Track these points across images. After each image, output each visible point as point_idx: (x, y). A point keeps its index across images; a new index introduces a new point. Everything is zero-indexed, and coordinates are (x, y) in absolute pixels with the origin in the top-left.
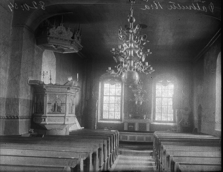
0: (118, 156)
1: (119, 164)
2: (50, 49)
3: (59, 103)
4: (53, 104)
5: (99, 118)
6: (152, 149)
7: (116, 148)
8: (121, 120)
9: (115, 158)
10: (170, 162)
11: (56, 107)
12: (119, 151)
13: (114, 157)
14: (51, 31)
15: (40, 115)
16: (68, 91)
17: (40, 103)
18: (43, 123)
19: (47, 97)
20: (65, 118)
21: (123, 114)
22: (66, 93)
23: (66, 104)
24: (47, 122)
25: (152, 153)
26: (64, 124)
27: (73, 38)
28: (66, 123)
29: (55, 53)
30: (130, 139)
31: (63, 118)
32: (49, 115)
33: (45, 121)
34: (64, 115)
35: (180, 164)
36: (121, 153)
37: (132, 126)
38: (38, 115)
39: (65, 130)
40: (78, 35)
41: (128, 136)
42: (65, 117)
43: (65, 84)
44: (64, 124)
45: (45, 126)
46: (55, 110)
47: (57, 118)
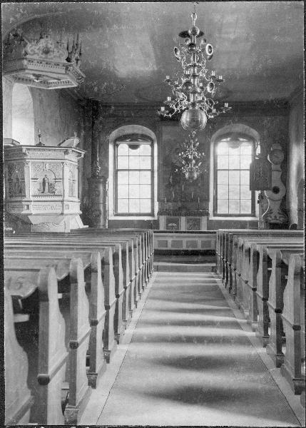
0: (133, 314)
1: (156, 282)
2: (24, 83)
3: (51, 178)
4: (40, 180)
5: (111, 211)
6: (215, 261)
7: (128, 290)
8: (152, 214)
9: (148, 278)
10: (252, 254)
11: (47, 184)
12: (154, 266)
13: (137, 292)
14: (29, 48)
15: (19, 199)
16: (66, 157)
17: (18, 179)
18: (25, 212)
19: (30, 167)
20: (63, 204)
21: (156, 204)
22: (63, 161)
23: (63, 179)
24: (33, 210)
25: (213, 267)
26: (62, 214)
27: (68, 60)
28: (65, 212)
29: (32, 89)
30: (172, 246)
31: (60, 203)
32: (36, 199)
33: (28, 208)
34: (61, 198)
35: (268, 247)
36: (158, 269)
37: (174, 225)
38: (13, 199)
39: (62, 223)
40: (77, 55)
41: (170, 240)
42: (62, 201)
43: (60, 144)
44: (62, 214)
45: (29, 217)
46: (44, 189)
47: (43, 203)
